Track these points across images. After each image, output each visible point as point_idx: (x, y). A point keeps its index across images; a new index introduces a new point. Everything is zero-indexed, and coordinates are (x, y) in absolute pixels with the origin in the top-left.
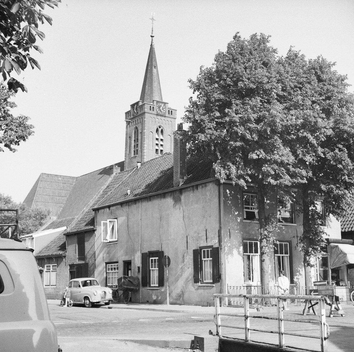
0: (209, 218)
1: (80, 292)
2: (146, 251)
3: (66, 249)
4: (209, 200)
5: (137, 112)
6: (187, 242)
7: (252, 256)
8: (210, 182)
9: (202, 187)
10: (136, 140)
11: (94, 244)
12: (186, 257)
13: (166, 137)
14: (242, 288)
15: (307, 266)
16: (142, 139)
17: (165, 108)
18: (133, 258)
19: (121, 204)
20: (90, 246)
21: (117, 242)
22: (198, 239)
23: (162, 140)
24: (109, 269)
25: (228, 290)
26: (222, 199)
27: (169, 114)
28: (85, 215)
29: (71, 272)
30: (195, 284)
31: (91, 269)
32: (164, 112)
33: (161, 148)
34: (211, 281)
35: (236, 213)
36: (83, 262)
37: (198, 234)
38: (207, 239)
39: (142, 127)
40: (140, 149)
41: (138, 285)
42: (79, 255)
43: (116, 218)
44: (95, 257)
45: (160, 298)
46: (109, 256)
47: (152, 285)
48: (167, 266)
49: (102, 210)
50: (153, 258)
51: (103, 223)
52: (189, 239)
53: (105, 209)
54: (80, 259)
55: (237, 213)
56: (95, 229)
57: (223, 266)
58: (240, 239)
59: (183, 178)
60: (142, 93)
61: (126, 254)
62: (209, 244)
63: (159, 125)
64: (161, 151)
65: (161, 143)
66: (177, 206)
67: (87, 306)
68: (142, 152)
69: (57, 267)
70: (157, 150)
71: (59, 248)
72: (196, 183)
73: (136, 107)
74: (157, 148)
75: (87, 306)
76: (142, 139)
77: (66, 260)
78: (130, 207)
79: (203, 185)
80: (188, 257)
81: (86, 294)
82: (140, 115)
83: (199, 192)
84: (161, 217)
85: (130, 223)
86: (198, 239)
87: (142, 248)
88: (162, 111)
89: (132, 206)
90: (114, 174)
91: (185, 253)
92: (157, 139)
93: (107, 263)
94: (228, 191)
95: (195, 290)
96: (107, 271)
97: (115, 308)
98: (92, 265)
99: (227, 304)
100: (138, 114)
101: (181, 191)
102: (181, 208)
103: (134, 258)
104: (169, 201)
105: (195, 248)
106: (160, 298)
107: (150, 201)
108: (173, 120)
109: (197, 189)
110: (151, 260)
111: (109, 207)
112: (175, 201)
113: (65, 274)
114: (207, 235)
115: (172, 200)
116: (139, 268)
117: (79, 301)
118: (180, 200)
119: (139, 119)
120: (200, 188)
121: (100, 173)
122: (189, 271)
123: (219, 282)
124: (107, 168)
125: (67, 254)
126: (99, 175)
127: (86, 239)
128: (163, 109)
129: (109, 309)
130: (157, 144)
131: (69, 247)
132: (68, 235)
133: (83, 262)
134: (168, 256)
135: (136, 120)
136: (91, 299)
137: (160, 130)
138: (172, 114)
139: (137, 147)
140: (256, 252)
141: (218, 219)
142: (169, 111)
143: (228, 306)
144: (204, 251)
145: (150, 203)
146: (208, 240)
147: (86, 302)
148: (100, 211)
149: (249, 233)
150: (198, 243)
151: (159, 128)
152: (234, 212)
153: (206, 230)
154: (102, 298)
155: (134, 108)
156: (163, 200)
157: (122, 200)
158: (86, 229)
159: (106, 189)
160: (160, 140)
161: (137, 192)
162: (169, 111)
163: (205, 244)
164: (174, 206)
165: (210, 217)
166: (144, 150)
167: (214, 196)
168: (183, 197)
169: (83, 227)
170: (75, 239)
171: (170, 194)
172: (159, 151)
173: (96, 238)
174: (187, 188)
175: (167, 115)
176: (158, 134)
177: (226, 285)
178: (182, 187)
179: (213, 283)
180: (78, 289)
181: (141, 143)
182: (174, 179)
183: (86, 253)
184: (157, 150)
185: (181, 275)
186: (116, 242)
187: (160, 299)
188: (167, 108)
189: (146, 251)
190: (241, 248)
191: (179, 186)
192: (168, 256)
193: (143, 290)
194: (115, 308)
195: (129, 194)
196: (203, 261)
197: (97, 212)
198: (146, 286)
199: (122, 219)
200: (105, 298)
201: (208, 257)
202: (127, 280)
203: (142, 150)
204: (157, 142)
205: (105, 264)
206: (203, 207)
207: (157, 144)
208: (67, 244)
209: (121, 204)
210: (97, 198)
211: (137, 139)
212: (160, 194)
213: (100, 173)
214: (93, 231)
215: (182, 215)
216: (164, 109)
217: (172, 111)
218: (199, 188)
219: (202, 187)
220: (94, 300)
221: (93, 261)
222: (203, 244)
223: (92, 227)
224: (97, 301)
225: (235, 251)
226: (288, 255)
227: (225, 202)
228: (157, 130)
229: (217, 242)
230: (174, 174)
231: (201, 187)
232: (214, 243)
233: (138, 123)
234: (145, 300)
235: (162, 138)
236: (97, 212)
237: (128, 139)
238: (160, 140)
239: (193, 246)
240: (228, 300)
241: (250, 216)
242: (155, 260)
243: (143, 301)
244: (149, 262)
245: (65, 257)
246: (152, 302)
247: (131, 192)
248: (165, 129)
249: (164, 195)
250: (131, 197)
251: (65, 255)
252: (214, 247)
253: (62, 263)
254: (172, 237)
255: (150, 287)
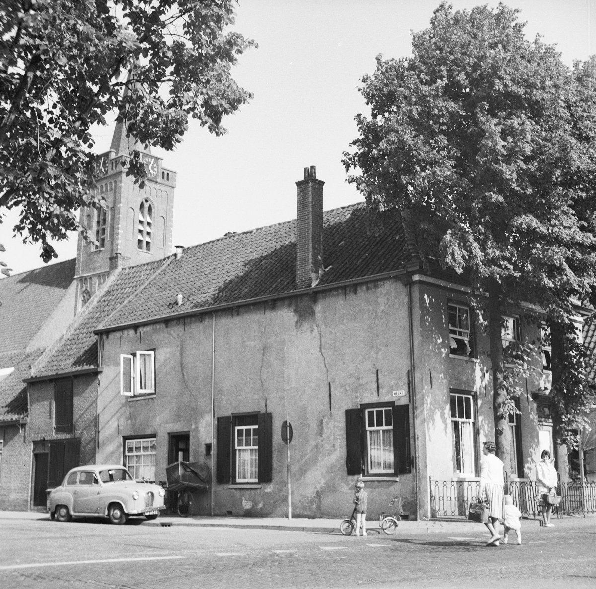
0: (383, 348)
1: (99, 493)
2: (227, 412)
3: (27, 410)
4: (384, 314)
5: (105, 170)
6: (330, 395)
7: (462, 423)
8: (388, 278)
9: (367, 289)
10: (101, 221)
11: (97, 399)
12: (328, 424)
13: (156, 220)
14: (449, 485)
15: (561, 445)
16: (113, 219)
17: (158, 166)
18: (193, 426)
19: (167, 322)
20: (86, 405)
21: (154, 396)
22: (358, 388)
23: (149, 224)
24: (130, 450)
25: (430, 491)
26: (417, 312)
27: (163, 178)
28: (65, 345)
29: (36, 456)
30: (350, 478)
31: (87, 449)
32: (155, 173)
33: (148, 239)
34: (392, 471)
35: (440, 341)
36: (68, 436)
37: (358, 379)
38: (378, 388)
39: (115, 198)
40: (110, 237)
41: (208, 481)
42: (57, 422)
43: (154, 350)
44: (97, 425)
45: (260, 505)
46: (134, 424)
47: (238, 480)
48: (288, 441)
49: (118, 334)
50: (244, 427)
51: (124, 358)
52: (335, 389)
53: (125, 332)
54: (58, 430)
55: (441, 340)
56: (99, 370)
57: (419, 442)
58: (445, 391)
59: (317, 272)
60: (114, 137)
61: (178, 418)
62: (385, 398)
63: (145, 196)
64: (148, 243)
65: (148, 229)
66: (306, 326)
67: (116, 521)
68: (112, 243)
69: (5, 446)
70: (140, 242)
71: (7, 409)
72: (355, 280)
73: (104, 162)
74: (140, 237)
75: (116, 521)
76: (113, 219)
77: (25, 431)
78: (187, 328)
79: (369, 285)
80: (331, 425)
81: (113, 497)
82: (110, 177)
83: (361, 300)
84: (264, 348)
85: (188, 360)
86: (358, 388)
87: (218, 407)
88: (152, 171)
89: (193, 326)
90: (119, 269)
91: (324, 417)
92: (141, 222)
93: (125, 438)
94: (426, 297)
95: (349, 489)
96: (127, 454)
97: (179, 525)
98: (90, 441)
99: (429, 514)
100: (107, 173)
101: (315, 296)
102: (316, 330)
103: (197, 427)
104: (286, 316)
105: (350, 406)
106: (260, 505)
107: (238, 315)
108: (169, 189)
109: (355, 293)
110: (239, 430)
111: (135, 327)
112: (300, 316)
113: (22, 460)
114: (380, 381)
115: (292, 314)
116: (208, 447)
117: (96, 512)
118: (313, 313)
119: (104, 185)
120: (361, 292)
121: (23, 281)
122: (338, 453)
123: (410, 472)
124: (35, 272)
125: (28, 419)
126: (19, 284)
127: (75, 391)
128: (153, 169)
129: (164, 528)
130: (140, 231)
131: (34, 406)
132: (34, 383)
133: (68, 436)
134: (289, 423)
135: (104, 185)
136: (126, 506)
137: (146, 205)
138: (168, 179)
139: (104, 233)
140: (468, 417)
141: (406, 350)
142: (163, 173)
143: (431, 520)
144: (371, 414)
145: (237, 320)
146: (381, 390)
147: (112, 512)
148: (111, 336)
149: (458, 379)
150: (357, 397)
151: (144, 202)
152: (436, 340)
153: (377, 371)
154: (147, 505)
155: (100, 163)
156: (270, 315)
157: (166, 313)
158: (78, 371)
159: (105, 296)
160: (145, 224)
161: (200, 299)
162: (163, 173)
163: (374, 399)
164: (298, 325)
165: (387, 346)
166: (117, 239)
167: (397, 306)
168: (319, 308)
169: (67, 367)
170: (51, 390)
171: (287, 302)
172: (144, 244)
173: (100, 389)
174: (330, 290)
175: (160, 180)
176: (142, 213)
177: (426, 478)
178: (320, 289)
179: (395, 475)
180: (94, 488)
181: (113, 227)
182: (299, 272)
183: (76, 416)
184: (140, 242)
185: (316, 460)
186: (152, 396)
187: (261, 509)
188: (160, 167)
189: (228, 413)
190: (448, 408)
191: (310, 285)
192: (289, 423)
193: (219, 492)
194: (179, 525)
195: (180, 303)
196: (368, 433)
197: (104, 337)
198: (228, 482)
199: (163, 353)
200: (152, 505)
201: (380, 424)
202: (189, 470)
203: (113, 239)
204: (141, 228)
205: (121, 439)
206: (370, 327)
207: (140, 231)
208: (31, 400)
209: (167, 322)
210: (87, 312)
211: (104, 220)
212: (265, 302)
213: (23, 281)
214: (96, 374)
215: (317, 343)
216: (156, 169)
217: (168, 174)
218: (359, 290)
219: (367, 289)
220: (132, 508)
221: (94, 433)
222: (370, 397)
223: (92, 367)
224: (140, 512)
225: (437, 416)
226: (514, 424)
227: (422, 321)
228: (142, 206)
229: (404, 394)
230: (298, 263)
231: (364, 288)
232: (400, 396)
233: (107, 190)
234: (224, 510)
235: (150, 221)
236: (104, 337)
237: (85, 218)
238: (145, 224)
239: (345, 403)
240: (431, 508)
241: (461, 349)
242: (248, 431)
243: (217, 511)
244: (234, 435)
245: (24, 425)
246: (241, 513)
247: (187, 299)
248: (155, 203)
249: (272, 304)
250: (187, 309)
251: (24, 422)
252: (396, 404)
253: (16, 438)
254: (293, 385)
255: (234, 483)
